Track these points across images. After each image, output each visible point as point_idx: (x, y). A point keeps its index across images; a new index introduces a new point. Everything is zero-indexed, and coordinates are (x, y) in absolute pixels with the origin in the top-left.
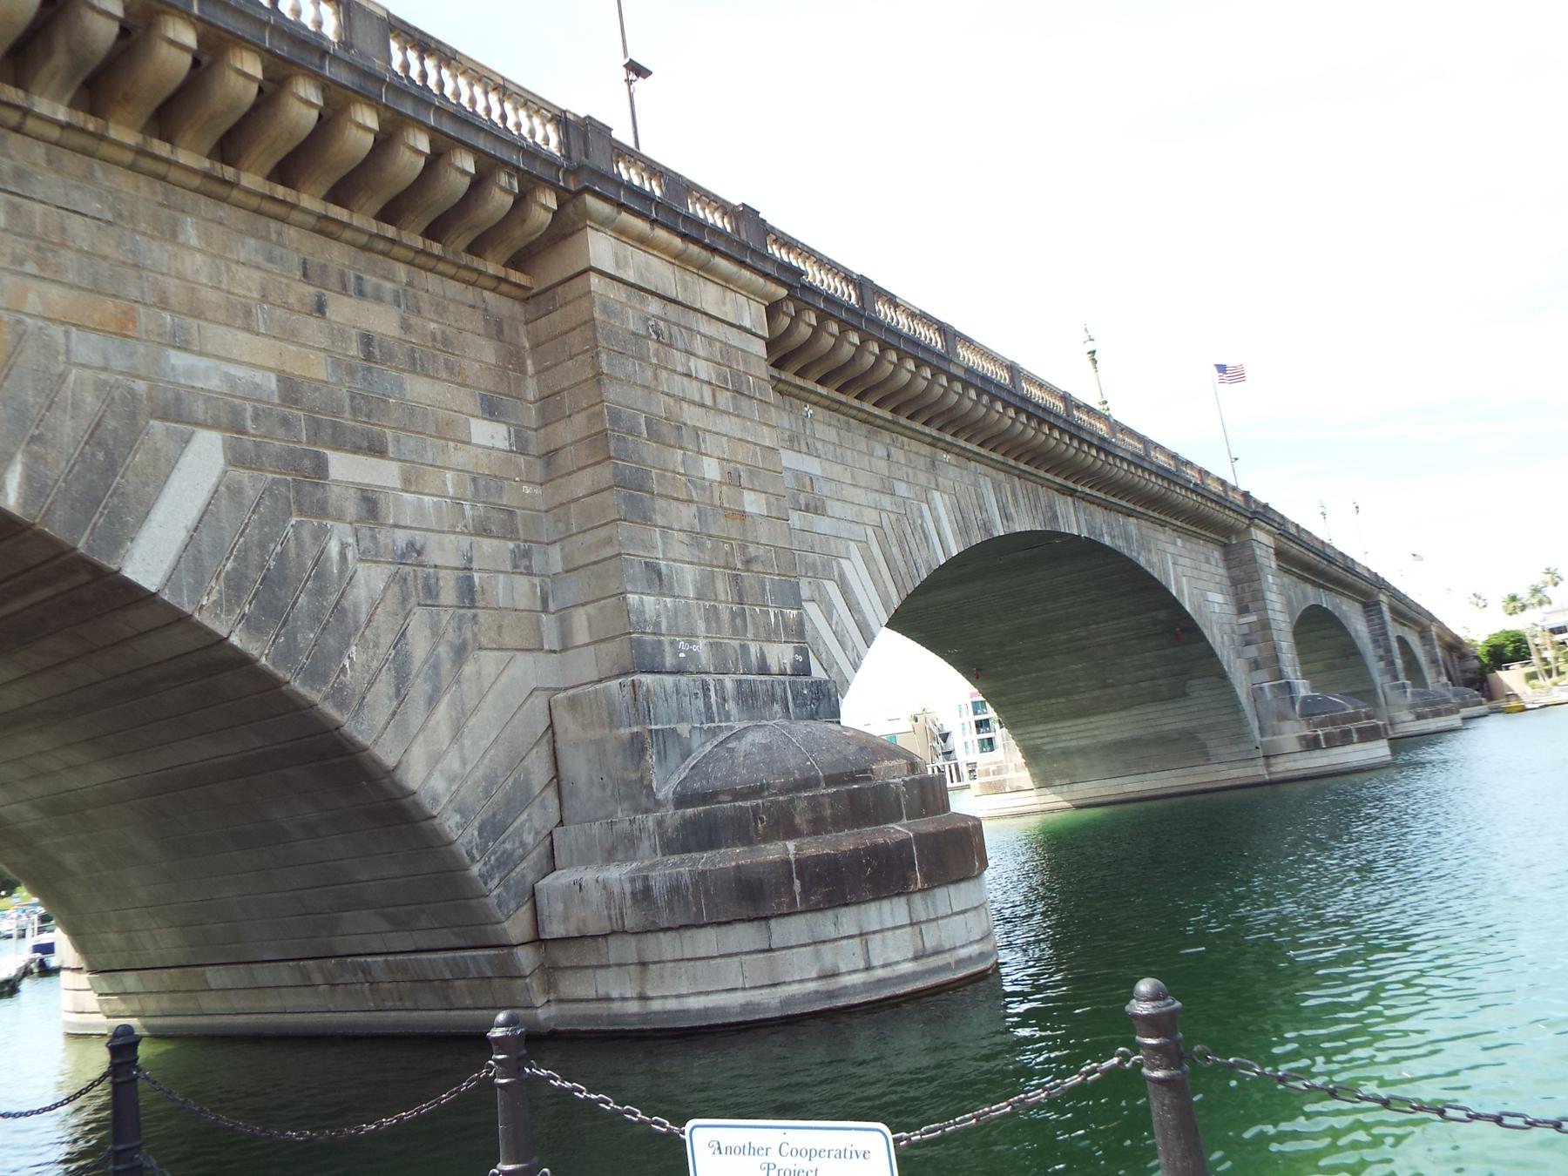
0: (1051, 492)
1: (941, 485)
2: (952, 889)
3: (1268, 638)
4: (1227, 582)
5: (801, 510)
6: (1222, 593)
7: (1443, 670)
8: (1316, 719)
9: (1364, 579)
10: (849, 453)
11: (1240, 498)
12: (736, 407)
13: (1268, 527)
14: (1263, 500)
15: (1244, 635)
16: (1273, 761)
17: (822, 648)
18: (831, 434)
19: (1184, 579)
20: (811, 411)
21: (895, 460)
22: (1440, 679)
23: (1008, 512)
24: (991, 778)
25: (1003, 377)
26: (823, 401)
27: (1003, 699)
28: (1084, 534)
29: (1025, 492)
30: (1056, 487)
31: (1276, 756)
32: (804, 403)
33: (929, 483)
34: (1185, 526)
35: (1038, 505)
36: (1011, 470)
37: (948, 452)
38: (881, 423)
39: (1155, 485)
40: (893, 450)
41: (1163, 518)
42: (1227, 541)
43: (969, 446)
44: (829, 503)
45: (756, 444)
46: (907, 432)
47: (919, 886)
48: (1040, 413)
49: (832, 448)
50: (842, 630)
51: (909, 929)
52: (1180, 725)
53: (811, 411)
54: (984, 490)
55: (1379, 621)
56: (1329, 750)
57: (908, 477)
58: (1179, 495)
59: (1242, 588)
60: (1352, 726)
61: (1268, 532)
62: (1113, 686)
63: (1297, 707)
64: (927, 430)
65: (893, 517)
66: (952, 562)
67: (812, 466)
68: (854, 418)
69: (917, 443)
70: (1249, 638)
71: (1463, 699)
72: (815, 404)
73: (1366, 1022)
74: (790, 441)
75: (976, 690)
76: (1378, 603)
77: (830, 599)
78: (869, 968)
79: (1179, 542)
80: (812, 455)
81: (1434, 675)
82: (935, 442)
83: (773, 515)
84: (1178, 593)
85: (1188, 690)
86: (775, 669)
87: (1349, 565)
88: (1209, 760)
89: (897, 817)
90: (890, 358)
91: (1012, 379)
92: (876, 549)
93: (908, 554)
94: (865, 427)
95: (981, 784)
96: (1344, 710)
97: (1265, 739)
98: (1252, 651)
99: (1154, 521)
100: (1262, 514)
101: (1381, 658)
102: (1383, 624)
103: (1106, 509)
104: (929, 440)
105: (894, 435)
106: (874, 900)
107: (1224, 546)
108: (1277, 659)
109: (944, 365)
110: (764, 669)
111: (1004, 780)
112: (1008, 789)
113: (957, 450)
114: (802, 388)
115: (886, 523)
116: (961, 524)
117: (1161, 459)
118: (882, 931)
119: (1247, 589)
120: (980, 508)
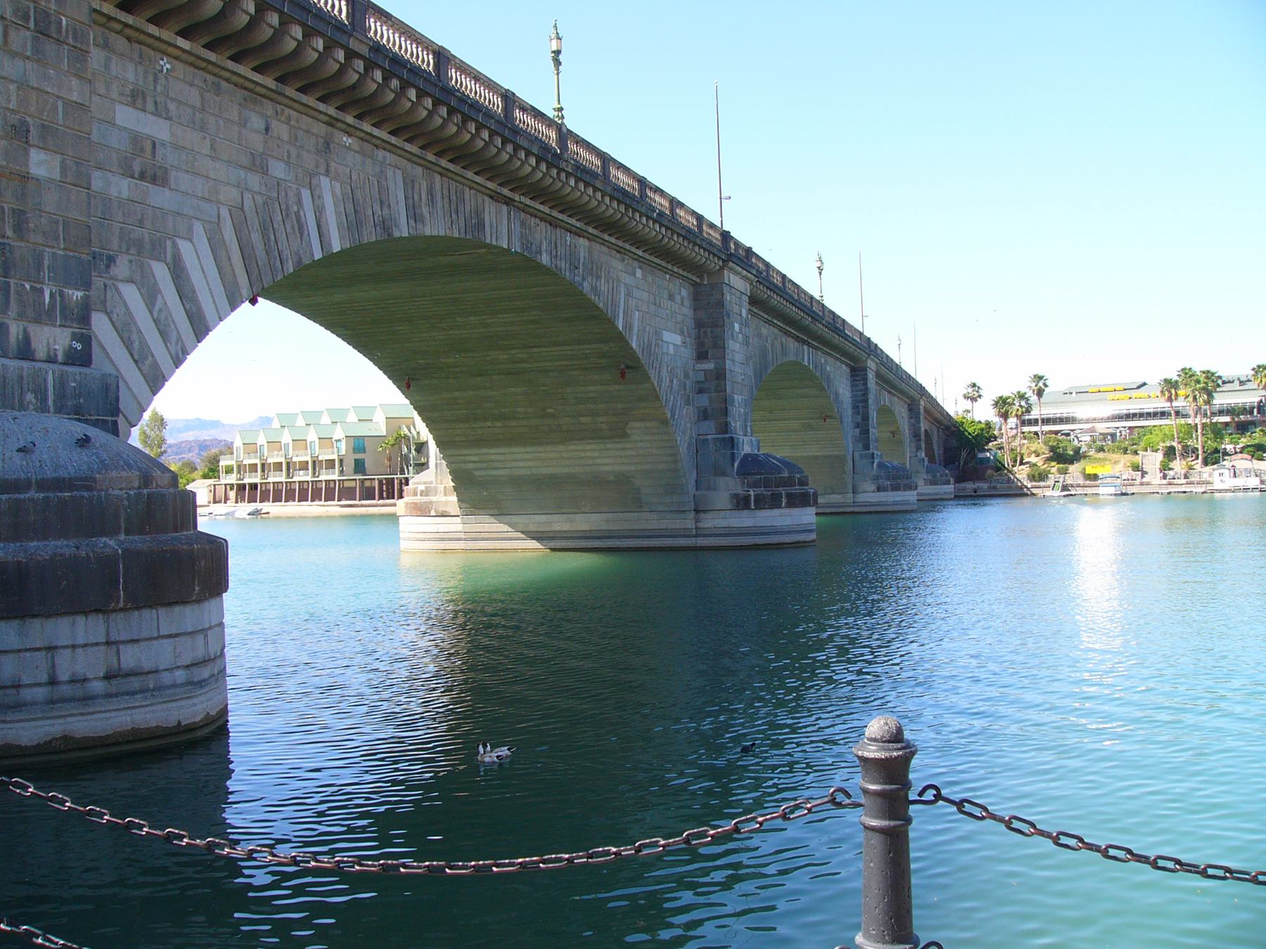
0: (480, 196)
1: (332, 169)
2: (162, 611)
3: (721, 389)
4: (690, 323)
5: (133, 177)
6: (682, 333)
7: (923, 445)
8: (751, 479)
9: (853, 342)
10: (212, 120)
11: (718, 237)
12: (36, 50)
13: (745, 272)
14: (748, 245)
15: (698, 382)
16: (702, 515)
17: (135, 336)
18: (193, 96)
19: (637, 313)
20: (168, 66)
21: (275, 135)
22: (919, 454)
23: (418, 211)
24: (419, 499)
25: (427, 62)
26: (184, 56)
27: (436, 414)
28: (516, 247)
29: (446, 192)
30: (490, 192)
31: (705, 511)
32: (159, 55)
33: (317, 167)
34: (647, 256)
35: (461, 208)
36: (430, 165)
37: (350, 135)
38: (263, 91)
39: (612, 209)
40: (274, 124)
41: (620, 244)
42: (698, 280)
43: (376, 132)
44: (173, 174)
45: (57, 97)
46: (296, 106)
47: (121, 605)
48: (466, 109)
49: (189, 111)
50: (166, 318)
51: (103, 648)
52: (616, 468)
53: (168, 66)
54: (391, 185)
55: (862, 388)
56: (757, 511)
57: (289, 157)
58: (639, 223)
59: (705, 333)
60: (783, 491)
61: (745, 278)
62: (553, 416)
63: (736, 465)
64: (322, 107)
65: (259, 199)
66: (330, 259)
67: (156, 128)
68: (227, 80)
69: (309, 120)
70: (702, 386)
71: (934, 476)
72: (176, 58)
73: (775, 790)
74: (133, 96)
75: (408, 402)
76: (865, 369)
77: (156, 283)
78: (53, 682)
79: (639, 273)
80: (160, 116)
81: (914, 449)
82: (334, 122)
83: (68, 180)
84: (625, 327)
85: (629, 431)
86: (41, 353)
87: (836, 324)
88: (641, 507)
89: (114, 532)
90: (269, 20)
91: (437, 66)
92: (229, 234)
93: (273, 243)
94: (240, 93)
95: (407, 503)
96: (780, 473)
97: (698, 493)
98: (704, 401)
99: (611, 246)
100: (745, 258)
101: (857, 426)
102: (866, 392)
103: (551, 224)
104: (325, 118)
105: (279, 107)
106: (67, 613)
107: (695, 284)
108: (725, 412)
109: (343, 39)
110: (25, 352)
111: (431, 503)
112: (433, 513)
113: (362, 135)
114: (158, 39)
115: (248, 204)
116: (352, 217)
117: (623, 180)
118: (74, 647)
119: (709, 335)
120: (382, 202)
